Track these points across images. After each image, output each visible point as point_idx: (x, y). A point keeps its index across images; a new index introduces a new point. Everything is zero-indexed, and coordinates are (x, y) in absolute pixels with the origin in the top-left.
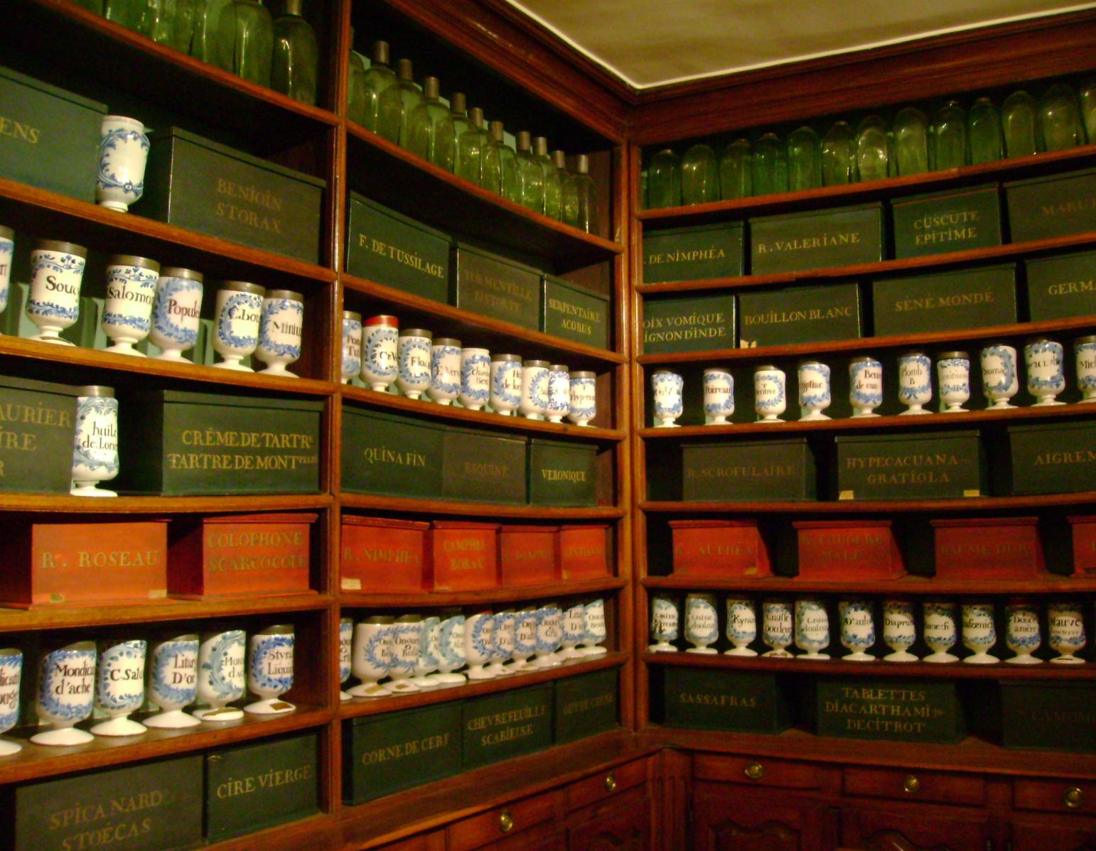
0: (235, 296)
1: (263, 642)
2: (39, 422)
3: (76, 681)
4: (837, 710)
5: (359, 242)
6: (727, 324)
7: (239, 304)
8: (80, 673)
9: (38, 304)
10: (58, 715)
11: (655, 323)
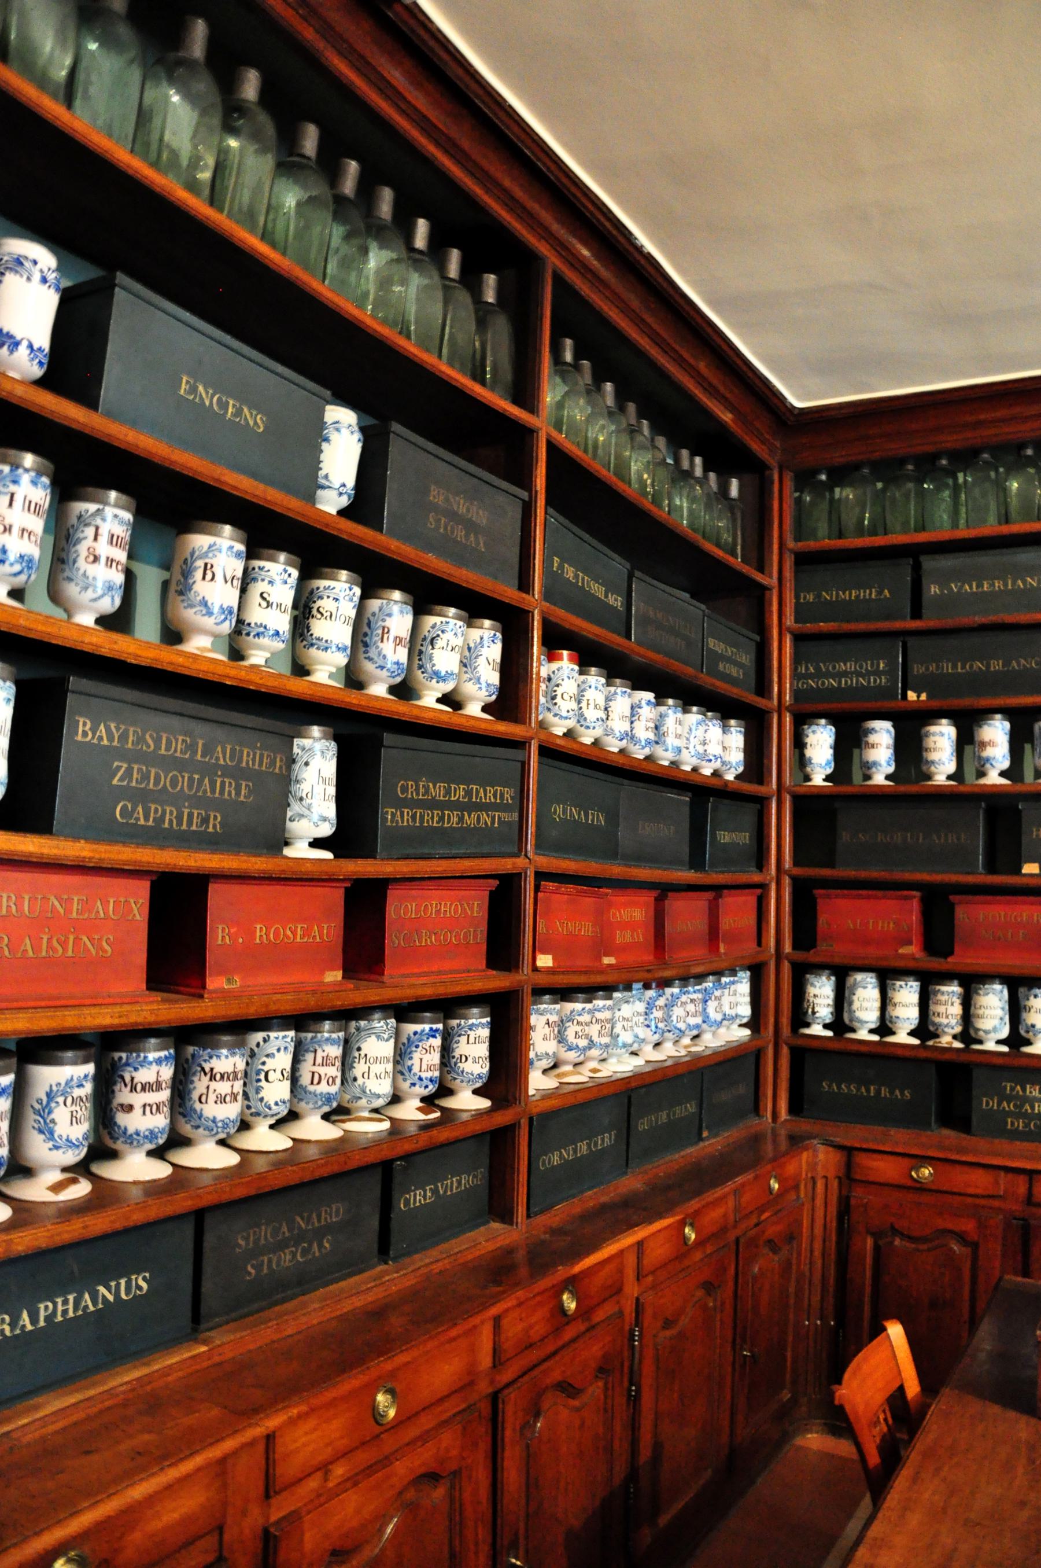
0: (439, 623)
1: (415, 1033)
2: (256, 767)
3: (223, 1087)
4: (995, 1107)
5: (553, 566)
6: (891, 672)
7: (443, 632)
8: (228, 1078)
9: (249, 624)
10: (201, 1130)
11: (807, 668)
